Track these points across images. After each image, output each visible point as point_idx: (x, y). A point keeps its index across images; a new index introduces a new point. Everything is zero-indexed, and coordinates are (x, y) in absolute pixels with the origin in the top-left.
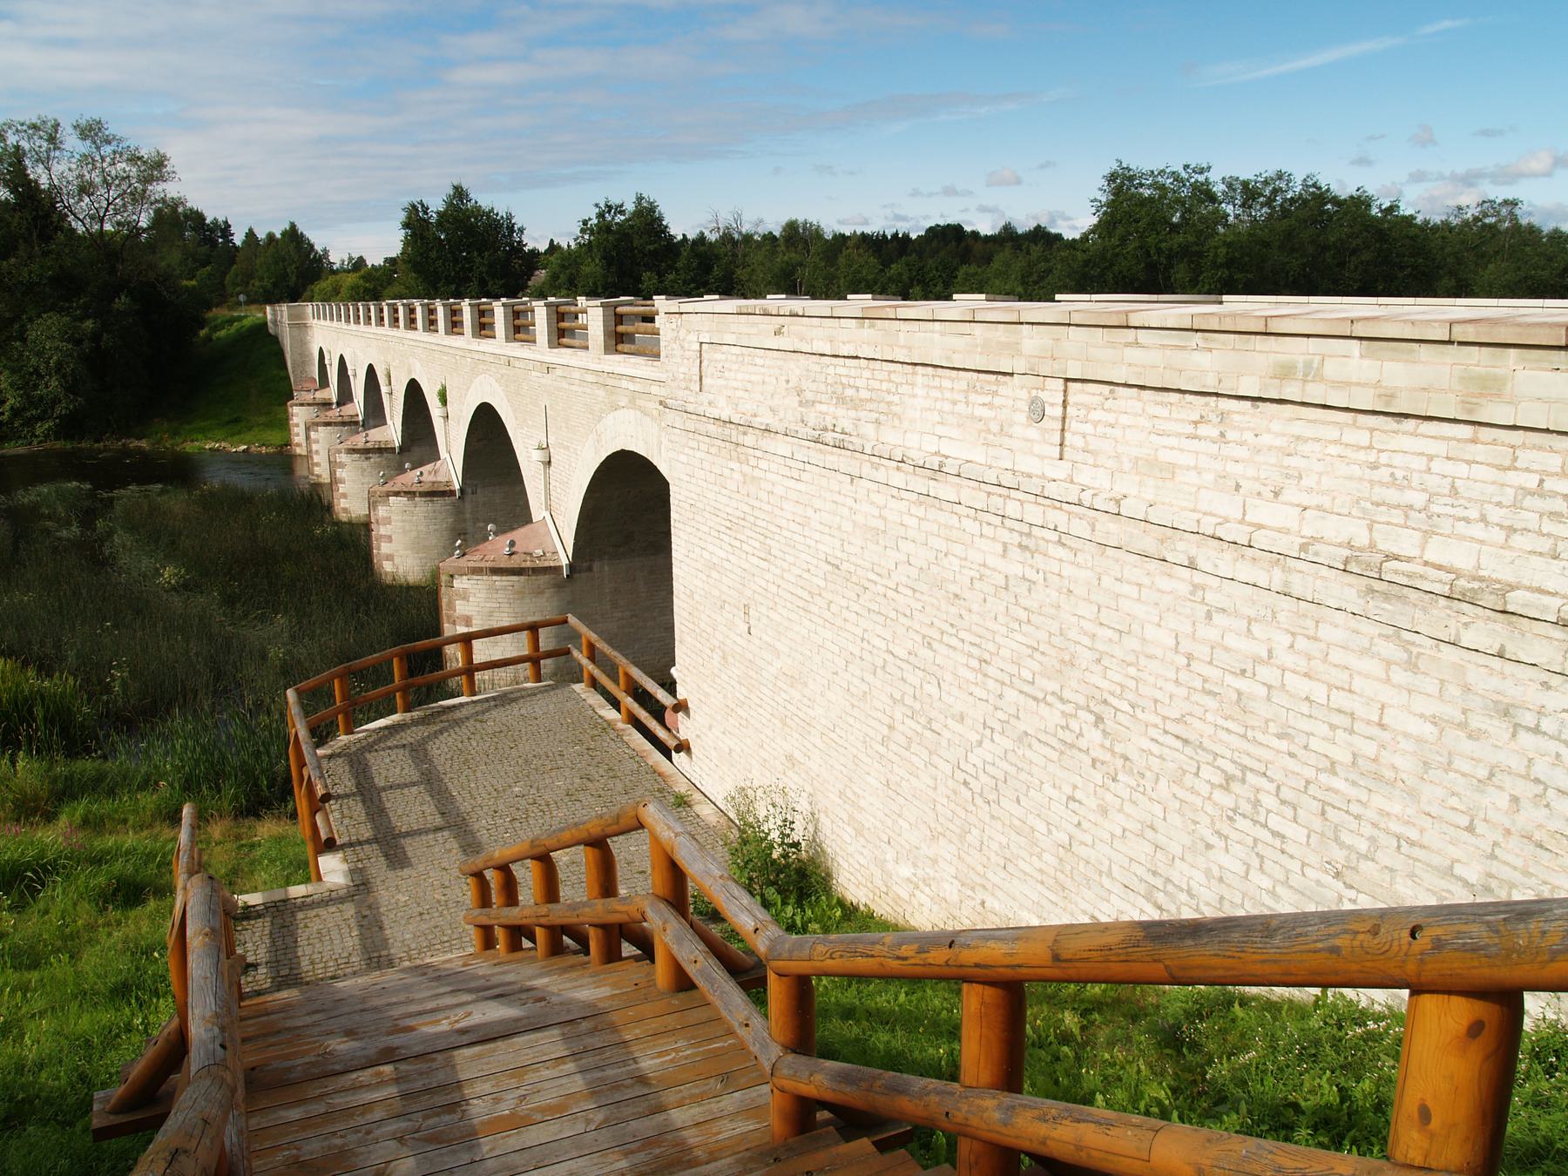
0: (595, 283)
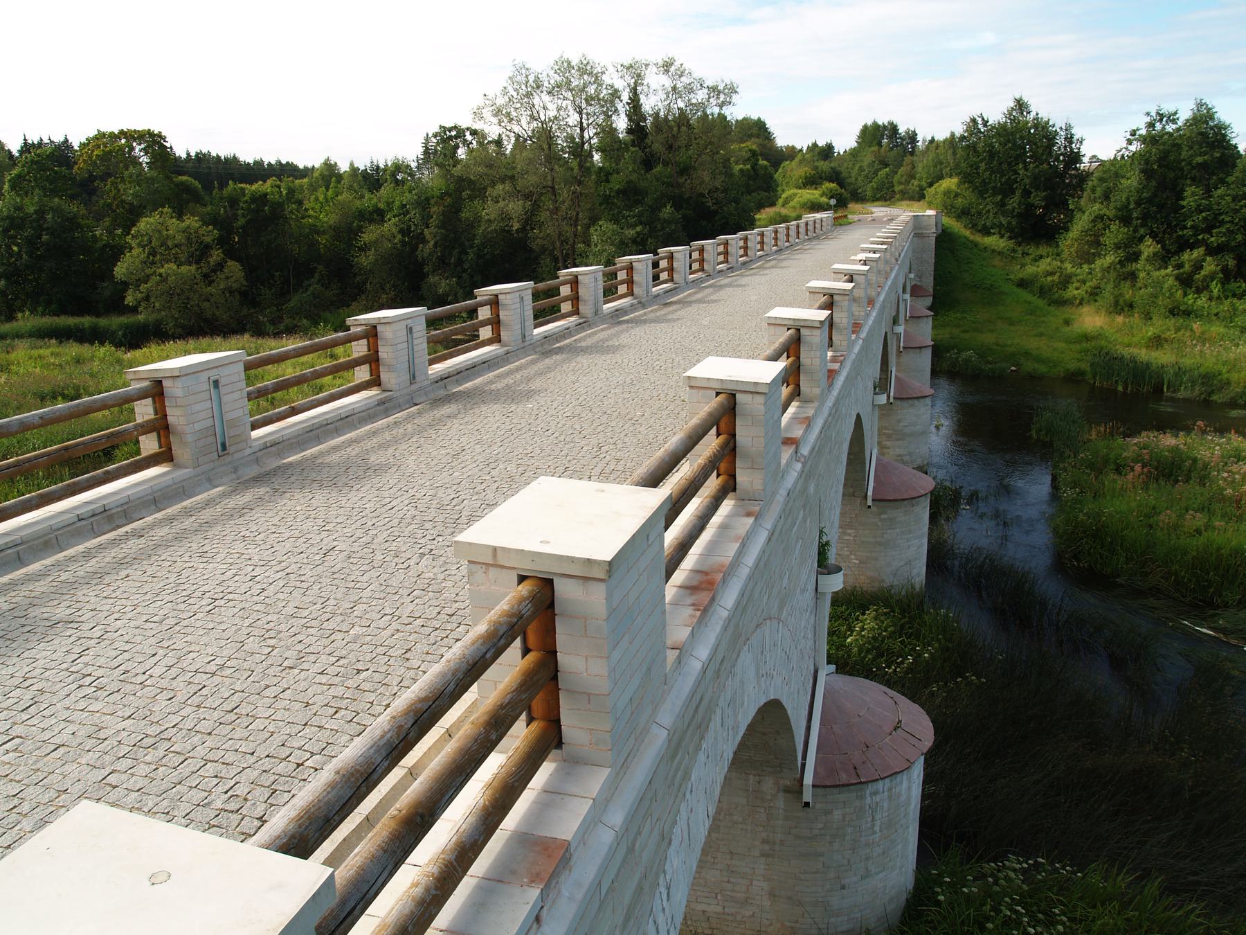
0: (1128, 199)
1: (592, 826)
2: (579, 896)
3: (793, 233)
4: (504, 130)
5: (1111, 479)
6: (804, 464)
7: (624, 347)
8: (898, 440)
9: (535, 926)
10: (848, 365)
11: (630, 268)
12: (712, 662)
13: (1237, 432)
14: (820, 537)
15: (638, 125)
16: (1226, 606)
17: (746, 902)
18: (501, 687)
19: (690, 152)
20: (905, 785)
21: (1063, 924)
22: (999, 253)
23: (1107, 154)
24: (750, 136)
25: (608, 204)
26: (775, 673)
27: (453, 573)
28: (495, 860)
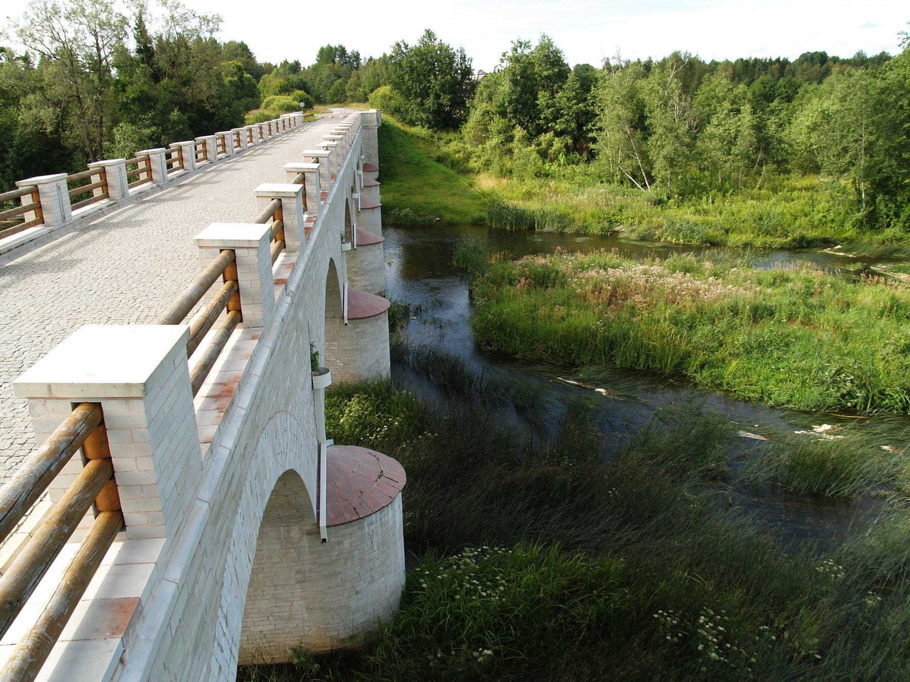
1: (157, 583)
2: (153, 636)
3: (274, 128)
4: (30, 49)
5: (507, 289)
6: (293, 298)
7: (148, 221)
8: (363, 275)
9: (120, 666)
10: (320, 223)
11: (148, 159)
12: (238, 448)
13: (581, 252)
14: (311, 350)
15: (145, 46)
16: (583, 364)
17: (290, 618)
18: (68, 491)
19: (189, 68)
20: (390, 514)
21: (503, 585)
22: (422, 139)
23: (489, 70)
24: (236, 55)
25: (127, 109)
26: (288, 451)
27: (21, 410)
28: (81, 624)
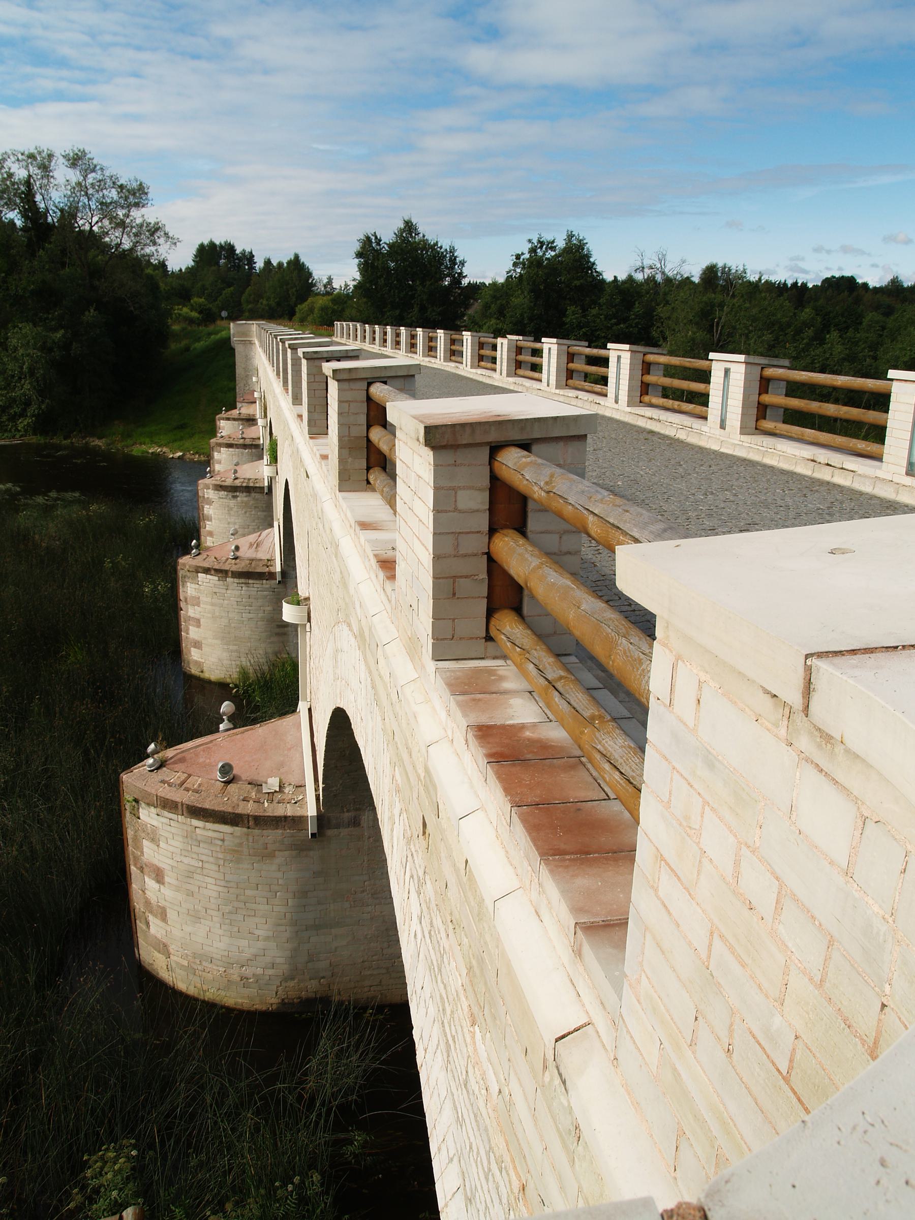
0: (522, 315)
